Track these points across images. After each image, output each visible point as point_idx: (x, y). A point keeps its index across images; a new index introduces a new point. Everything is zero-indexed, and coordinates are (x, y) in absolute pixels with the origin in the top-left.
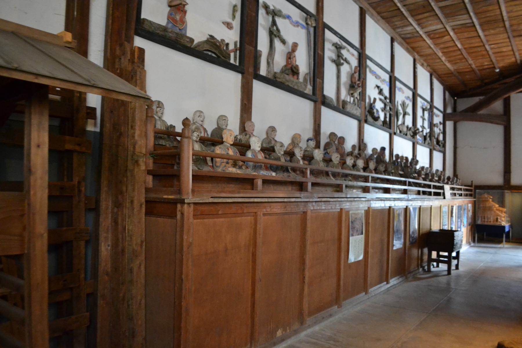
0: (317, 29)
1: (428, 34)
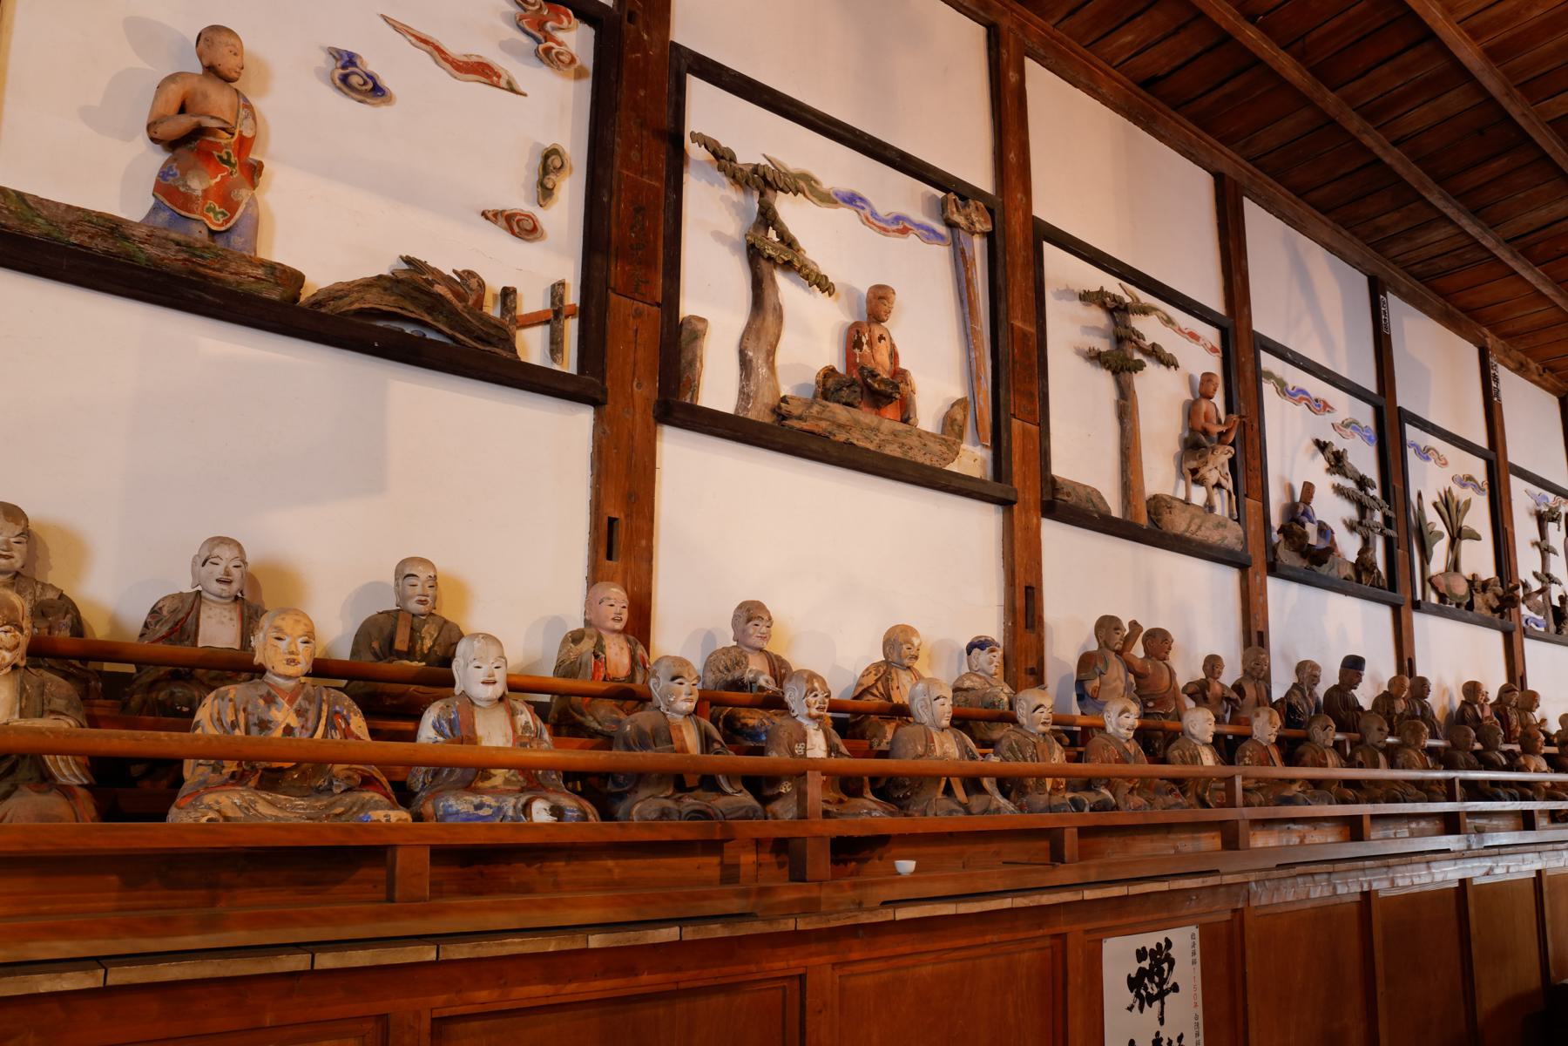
0: (999, 242)
1: (1524, 245)
